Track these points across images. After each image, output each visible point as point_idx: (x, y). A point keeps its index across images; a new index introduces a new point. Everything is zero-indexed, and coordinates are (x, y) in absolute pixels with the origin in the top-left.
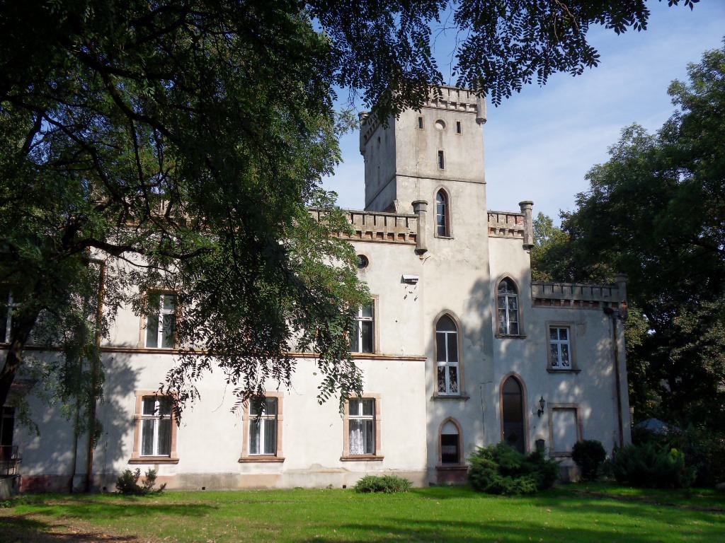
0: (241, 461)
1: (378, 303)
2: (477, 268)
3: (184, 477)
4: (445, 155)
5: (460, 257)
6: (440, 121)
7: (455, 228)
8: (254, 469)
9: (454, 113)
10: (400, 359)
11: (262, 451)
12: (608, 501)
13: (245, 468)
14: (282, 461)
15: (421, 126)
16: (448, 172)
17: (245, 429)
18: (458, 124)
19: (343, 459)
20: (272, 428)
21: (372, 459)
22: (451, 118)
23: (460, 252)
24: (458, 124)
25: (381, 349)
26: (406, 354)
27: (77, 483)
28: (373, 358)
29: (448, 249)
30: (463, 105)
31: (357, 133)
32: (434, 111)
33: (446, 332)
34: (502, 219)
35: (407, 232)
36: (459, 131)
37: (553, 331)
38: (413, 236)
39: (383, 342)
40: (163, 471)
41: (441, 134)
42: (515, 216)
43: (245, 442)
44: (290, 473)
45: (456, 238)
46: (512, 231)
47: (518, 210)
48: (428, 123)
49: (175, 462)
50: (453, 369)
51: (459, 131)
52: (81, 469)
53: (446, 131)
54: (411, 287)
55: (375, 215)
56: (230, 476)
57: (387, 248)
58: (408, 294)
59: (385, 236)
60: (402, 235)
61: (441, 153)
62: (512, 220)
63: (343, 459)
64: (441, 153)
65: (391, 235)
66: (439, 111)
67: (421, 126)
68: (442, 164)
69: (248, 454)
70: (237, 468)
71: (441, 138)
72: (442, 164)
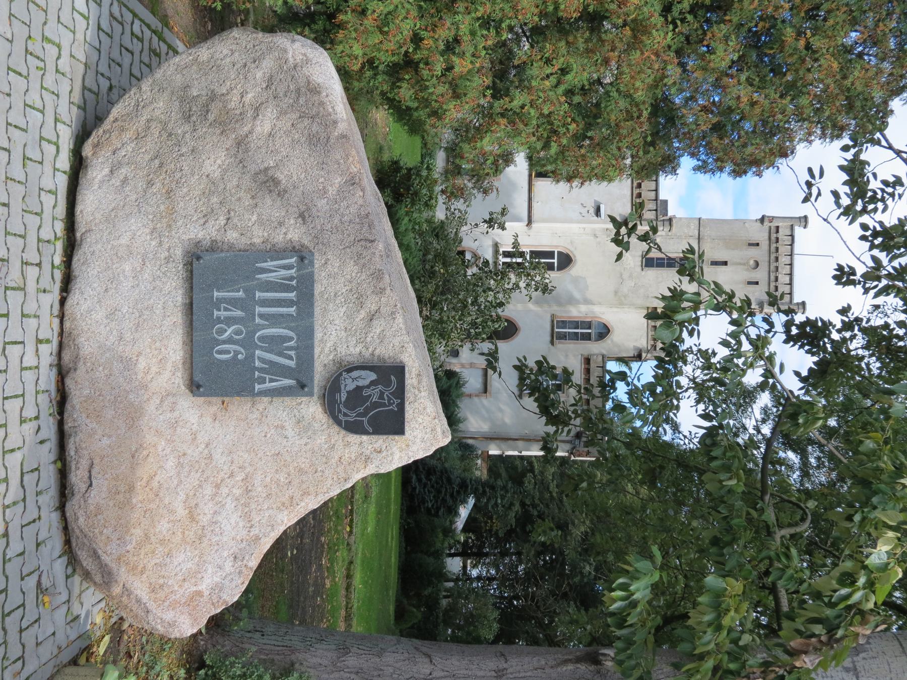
1: (561, 317)
2: (616, 293)
4: (723, 268)
5: (625, 276)
6: (757, 264)
9: (767, 279)
10: (530, 199)
15: (750, 245)
18: (757, 283)
23: (631, 276)
24: (757, 283)
25: (539, 183)
26: (534, 204)
28: (530, 176)
29: (632, 264)
30: (777, 259)
31: (729, 216)
32: (767, 259)
33: (555, 261)
36: (750, 283)
39: (543, 186)
41: (744, 264)
45: (643, 273)
48: (754, 252)
51: (750, 283)
53: (747, 270)
54: (592, 211)
55: (656, 210)
57: (628, 192)
58: (587, 209)
59: (638, 191)
61: (725, 263)
64: (725, 263)
66: (767, 264)
67: (750, 245)
68: (715, 263)
71: (740, 264)
72: (715, 263)
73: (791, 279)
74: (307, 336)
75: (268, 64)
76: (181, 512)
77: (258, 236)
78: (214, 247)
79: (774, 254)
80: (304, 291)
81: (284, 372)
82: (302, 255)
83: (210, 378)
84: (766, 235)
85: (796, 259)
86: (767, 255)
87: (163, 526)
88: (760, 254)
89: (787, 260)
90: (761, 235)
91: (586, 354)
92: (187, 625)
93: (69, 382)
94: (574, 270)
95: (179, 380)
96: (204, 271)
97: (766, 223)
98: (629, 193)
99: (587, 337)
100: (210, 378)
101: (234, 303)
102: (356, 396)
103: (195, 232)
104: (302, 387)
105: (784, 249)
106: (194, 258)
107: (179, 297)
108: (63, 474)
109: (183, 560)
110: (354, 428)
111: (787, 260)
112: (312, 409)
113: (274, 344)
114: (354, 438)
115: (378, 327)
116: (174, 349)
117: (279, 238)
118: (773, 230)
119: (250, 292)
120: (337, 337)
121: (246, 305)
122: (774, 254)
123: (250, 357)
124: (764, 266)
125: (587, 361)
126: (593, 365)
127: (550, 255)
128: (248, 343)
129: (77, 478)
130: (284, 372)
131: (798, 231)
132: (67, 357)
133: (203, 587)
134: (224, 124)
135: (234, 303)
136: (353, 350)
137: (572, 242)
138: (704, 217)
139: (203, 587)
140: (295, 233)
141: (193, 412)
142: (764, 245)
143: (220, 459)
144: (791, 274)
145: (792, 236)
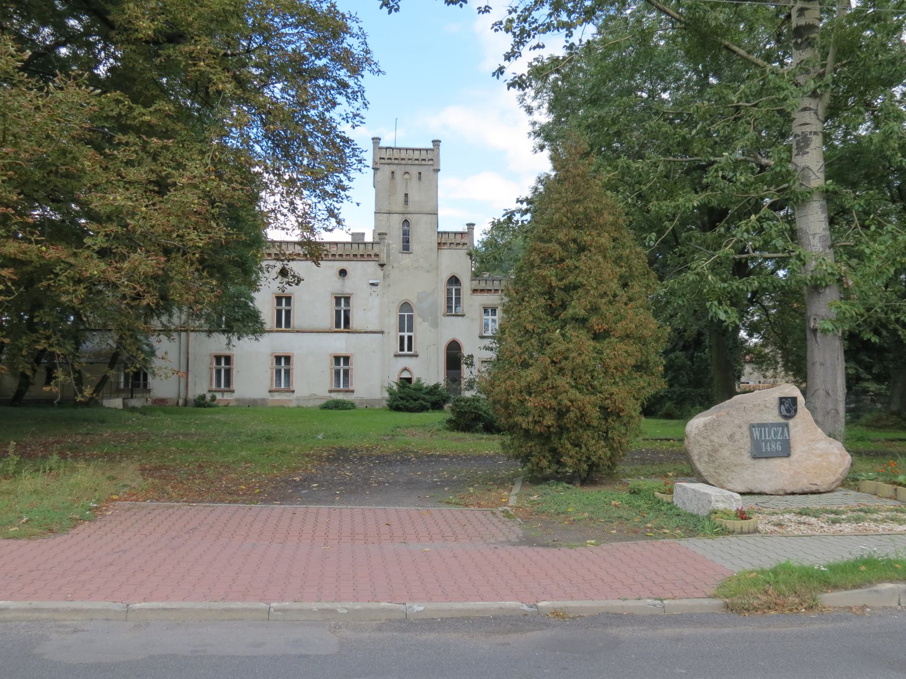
0: (270, 391)
3: (238, 400)
7: (413, 246)
8: (277, 397)
10: (366, 332)
11: (342, 387)
12: (459, 610)
13: (272, 396)
14: (293, 392)
16: (411, 208)
17: (272, 374)
19: (330, 391)
20: (228, 373)
21: (347, 391)
22: (414, 171)
26: (370, 329)
27: (181, 402)
28: (348, 332)
34: (452, 236)
35: (372, 253)
36: (420, 179)
37: (486, 311)
38: (376, 255)
40: (227, 396)
42: (427, 150)
43: (272, 381)
44: (298, 399)
46: (458, 244)
47: (431, 146)
48: (398, 175)
49: (233, 391)
50: (410, 338)
51: (420, 179)
52: (182, 395)
53: (410, 180)
54: (374, 288)
56: (263, 400)
60: (355, 255)
61: (406, 195)
62: (424, 153)
63: (330, 391)
64: (406, 195)
65: (362, 255)
68: (406, 202)
69: (334, 388)
70: (267, 395)
72: (406, 202)
73: (417, 150)
74: (773, 425)
75: (699, 438)
76: (820, 459)
77: (749, 439)
78: (751, 453)
79: (399, 162)
80: (762, 425)
81: (783, 431)
82: (752, 426)
83: (786, 451)
84: (387, 166)
85: (398, 146)
86: (399, 166)
87: (824, 464)
88: (399, 171)
89: (403, 153)
90: (386, 170)
91: (470, 292)
92: (849, 457)
93: (788, 492)
94: (413, 300)
95: (785, 460)
96: (758, 454)
97: (377, 166)
98: (360, 263)
99: (458, 292)
100: (786, 451)
101: (766, 445)
102: (788, 411)
103: (746, 458)
104: (787, 425)
105: (396, 154)
106: (755, 457)
107: (764, 461)
108: (813, 493)
109: (832, 458)
110: (796, 411)
111: (403, 153)
112: (791, 422)
113: (776, 434)
114: (799, 411)
115: (768, 405)
116: (778, 461)
117: (748, 433)
118: (383, 161)
119: (763, 441)
120: (773, 416)
121: (766, 442)
122: (399, 162)
123: (780, 440)
124: (408, 168)
125: (475, 291)
126: (479, 288)
127: (402, 318)
128: (776, 441)
129: (814, 488)
130: (783, 431)
131: (383, 144)
132: (781, 493)
133: (838, 452)
134: (715, 451)
135: (766, 445)
136: (776, 412)
137: (393, 303)
138: (374, 210)
139: (838, 452)
140: (745, 429)
141: (795, 456)
142: (393, 168)
143: (806, 448)
144: (413, 150)
145: (386, 148)
